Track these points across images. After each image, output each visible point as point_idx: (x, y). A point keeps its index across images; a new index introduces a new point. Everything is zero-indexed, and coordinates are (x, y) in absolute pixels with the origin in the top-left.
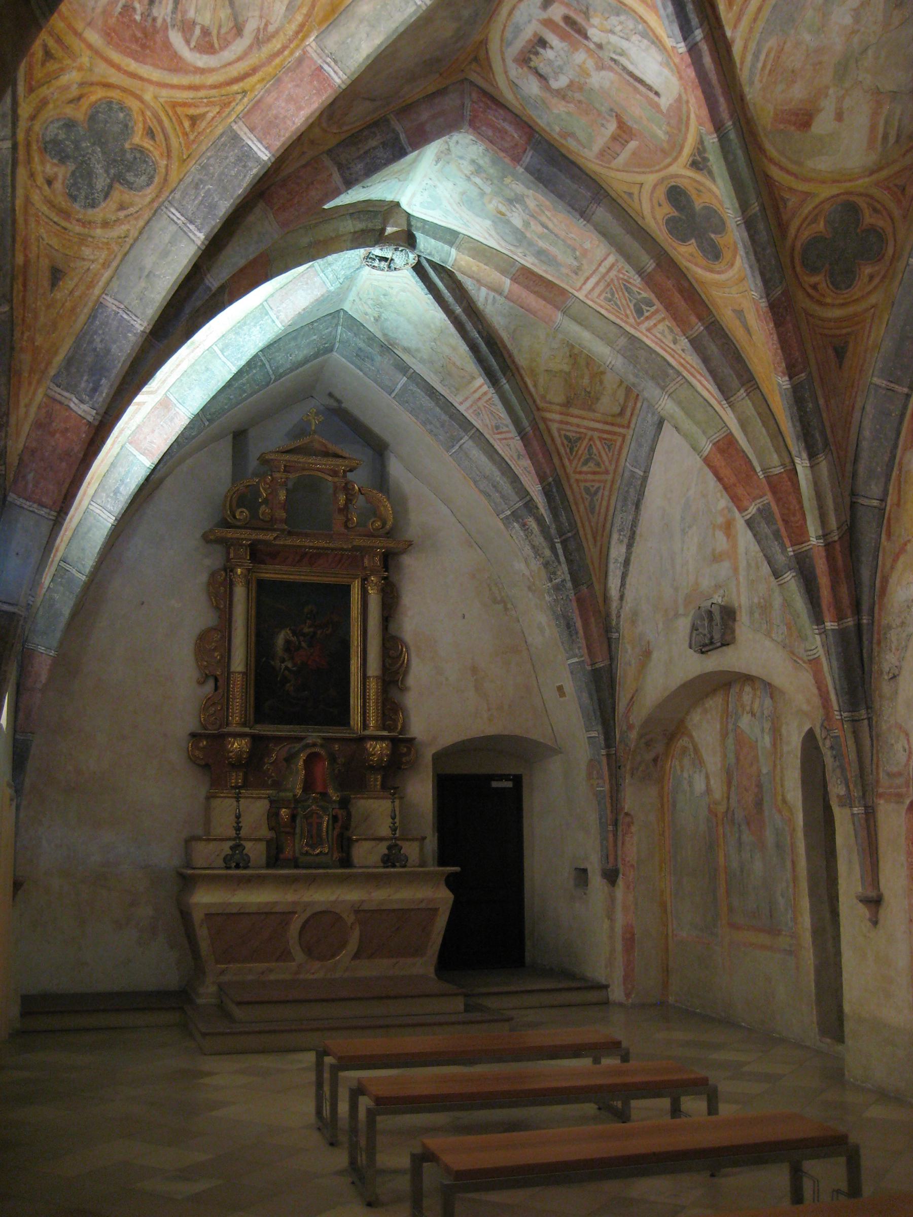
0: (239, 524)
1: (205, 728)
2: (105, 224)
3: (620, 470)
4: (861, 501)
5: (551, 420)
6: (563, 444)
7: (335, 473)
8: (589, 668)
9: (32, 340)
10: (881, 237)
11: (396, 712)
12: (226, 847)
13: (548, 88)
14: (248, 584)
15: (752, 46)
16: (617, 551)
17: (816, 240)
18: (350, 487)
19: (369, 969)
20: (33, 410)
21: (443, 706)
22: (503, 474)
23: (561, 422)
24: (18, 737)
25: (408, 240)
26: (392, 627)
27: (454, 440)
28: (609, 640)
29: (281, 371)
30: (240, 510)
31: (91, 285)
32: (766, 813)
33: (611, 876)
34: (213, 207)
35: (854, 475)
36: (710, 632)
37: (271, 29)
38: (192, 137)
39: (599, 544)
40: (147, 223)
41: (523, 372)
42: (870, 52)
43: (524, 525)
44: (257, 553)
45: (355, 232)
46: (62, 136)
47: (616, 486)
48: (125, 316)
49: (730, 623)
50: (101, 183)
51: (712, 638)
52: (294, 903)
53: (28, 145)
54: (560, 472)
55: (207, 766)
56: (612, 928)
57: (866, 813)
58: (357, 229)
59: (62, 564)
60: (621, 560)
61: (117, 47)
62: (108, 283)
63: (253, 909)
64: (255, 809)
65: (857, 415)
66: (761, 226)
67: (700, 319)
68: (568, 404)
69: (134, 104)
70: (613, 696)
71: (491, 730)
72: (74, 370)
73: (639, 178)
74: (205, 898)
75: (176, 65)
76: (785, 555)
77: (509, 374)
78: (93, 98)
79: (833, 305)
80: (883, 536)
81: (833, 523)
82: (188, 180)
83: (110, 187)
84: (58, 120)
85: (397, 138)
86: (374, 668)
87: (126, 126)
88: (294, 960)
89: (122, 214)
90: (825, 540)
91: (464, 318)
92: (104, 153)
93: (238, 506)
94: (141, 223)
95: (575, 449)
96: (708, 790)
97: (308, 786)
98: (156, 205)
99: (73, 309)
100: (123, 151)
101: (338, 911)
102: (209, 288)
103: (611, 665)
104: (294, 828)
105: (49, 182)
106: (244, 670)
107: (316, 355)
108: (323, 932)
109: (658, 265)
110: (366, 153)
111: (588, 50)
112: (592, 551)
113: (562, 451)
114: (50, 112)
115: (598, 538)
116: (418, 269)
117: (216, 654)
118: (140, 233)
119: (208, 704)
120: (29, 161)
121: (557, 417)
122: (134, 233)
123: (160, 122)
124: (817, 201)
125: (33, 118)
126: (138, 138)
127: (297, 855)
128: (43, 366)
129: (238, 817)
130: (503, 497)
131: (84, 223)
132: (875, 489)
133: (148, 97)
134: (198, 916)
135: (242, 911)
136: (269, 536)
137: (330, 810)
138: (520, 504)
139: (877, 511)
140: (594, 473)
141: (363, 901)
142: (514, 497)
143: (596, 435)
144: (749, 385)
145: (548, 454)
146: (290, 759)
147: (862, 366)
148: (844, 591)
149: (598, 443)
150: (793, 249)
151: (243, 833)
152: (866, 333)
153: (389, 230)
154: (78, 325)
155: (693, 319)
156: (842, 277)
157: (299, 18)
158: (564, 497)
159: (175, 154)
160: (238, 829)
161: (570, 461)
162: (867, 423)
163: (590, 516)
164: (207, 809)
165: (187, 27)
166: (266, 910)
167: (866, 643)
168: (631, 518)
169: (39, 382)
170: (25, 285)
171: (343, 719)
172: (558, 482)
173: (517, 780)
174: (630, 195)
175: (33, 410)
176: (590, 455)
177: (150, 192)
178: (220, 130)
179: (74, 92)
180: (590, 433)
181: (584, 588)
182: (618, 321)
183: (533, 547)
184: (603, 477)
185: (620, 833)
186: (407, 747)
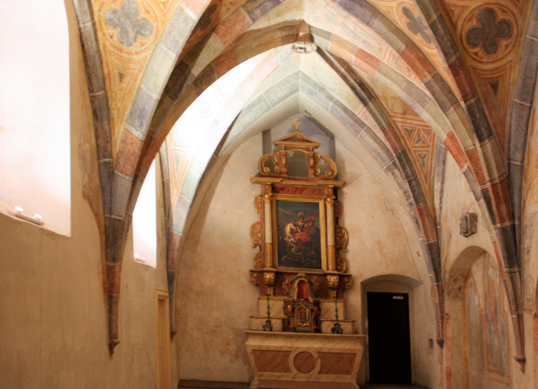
0: (265, 174)
1: (256, 268)
2: (137, 53)
3: (435, 145)
4: (513, 162)
5: (397, 122)
6: (405, 134)
7: (308, 150)
8: (426, 243)
9: (116, 105)
10: (508, 24)
11: (342, 262)
12: (264, 321)
14: (271, 203)
16: (437, 186)
17: (473, 30)
18: (316, 156)
20: (120, 135)
22: (382, 148)
23: (403, 122)
24: (169, 270)
25: (311, 39)
26: (340, 224)
27: (358, 132)
28: (437, 229)
29: (274, 102)
31: (136, 80)
32: (498, 316)
33: (441, 343)
34: (177, 42)
35: (509, 149)
36: (467, 227)
38: (165, 11)
39: (428, 182)
40: (154, 51)
41: (380, 99)
43: (393, 173)
44: (274, 189)
45: (282, 37)
46: (112, 17)
47: (435, 153)
48: (149, 93)
49: (475, 222)
50: (132, 35)
51: (467, 230)
52: (291, 347)
53: (100, 22)
56: (442, 368)
57: (518, 318)
58: (283, 35)
59: (181, 195)
60: (439, 190)
62: (142, 78)
63: (273, 349)
64: (277, 306)
65: (508, 118)
66: (439, 26)
67: (429, 72)
68: (405, 113)
70: (439, 257)
71: (388, 272)
72: (133, 117)
73: (390, 4)
74: (253, 343)
76: (478, 189)
77: (373, 100)
79: (488, 63)
80: (524, 180)
81: (496, 174)
82: (167, 30)
83: (136, 37)
84: (109, 10)
86: (331, 242)
87: (137, 10)
88: (291, 372)
89: (143, 48)
90: (491, 183)
91: (346, 74)
92: (130, 22)
93: (265, 166)
94: (151, 51)
95: (411, 135)
96: (479, 305)
97: (300, 295)
98: (155, 43)
99: (130, 91)
100: (138, 21)
101: (309, 351)
102: (193, 75)
103: (438, 242)
104: (294, 314)
105: (111, 37)
107: (291, 93)
108: (304, 360)
109: (407, 47)
110: (261, 4)
112: (425, 186)
113: (404, 136)
114: (105, 8)
115: (428, 179)
116: (319, 50)
117: (259, 235)
118: (152, 56)
119: (257, 257)
120: (102, 29)
122: (149, 56)
123: (151, 6)
124: (470, 10)
125: (99, 10)
126: (142, 15)
127: (296, 326)
128: (121, 116)
130: (382, 160)
131: (129, 53)
132: (518, 156)
134: (249, 350)
135: (268, 349)
138: (391, 163)
139: (519, 167)
140: (422, 147)
141: (322, 348)
142: (388, 160)
143: (421, 128)
144: (456, 105)
146: (292, 282)
147: (508, 93)
148: (504, 208)
149: (422, 132)
150: (461, 36)
151: (271, 315)
152: (508, 76)
153: (301, 34)
154: (133, 98)
155: (426, 73)
156: (491, 48)
158: (408, 160)
159: (159, 20)
160: (269, 314)
161: (410, 142)
162: (513, 122)
163: (423, 168)
164: (258, 305)
166: (278, 350)
167: (517, 234)
168: (441, 169)
169: (121, 122)
170: (110, 81)
172: (404, 152)
173: (406, 296)
174: (389, 12)
175: (120, 135)
176: (419, 138)
177: (152, 37)
180: (418, 127)
181: (421, 204)
182: (402, 74)
183: (398, 184)
184: (427, 149)
185: (444, 323)
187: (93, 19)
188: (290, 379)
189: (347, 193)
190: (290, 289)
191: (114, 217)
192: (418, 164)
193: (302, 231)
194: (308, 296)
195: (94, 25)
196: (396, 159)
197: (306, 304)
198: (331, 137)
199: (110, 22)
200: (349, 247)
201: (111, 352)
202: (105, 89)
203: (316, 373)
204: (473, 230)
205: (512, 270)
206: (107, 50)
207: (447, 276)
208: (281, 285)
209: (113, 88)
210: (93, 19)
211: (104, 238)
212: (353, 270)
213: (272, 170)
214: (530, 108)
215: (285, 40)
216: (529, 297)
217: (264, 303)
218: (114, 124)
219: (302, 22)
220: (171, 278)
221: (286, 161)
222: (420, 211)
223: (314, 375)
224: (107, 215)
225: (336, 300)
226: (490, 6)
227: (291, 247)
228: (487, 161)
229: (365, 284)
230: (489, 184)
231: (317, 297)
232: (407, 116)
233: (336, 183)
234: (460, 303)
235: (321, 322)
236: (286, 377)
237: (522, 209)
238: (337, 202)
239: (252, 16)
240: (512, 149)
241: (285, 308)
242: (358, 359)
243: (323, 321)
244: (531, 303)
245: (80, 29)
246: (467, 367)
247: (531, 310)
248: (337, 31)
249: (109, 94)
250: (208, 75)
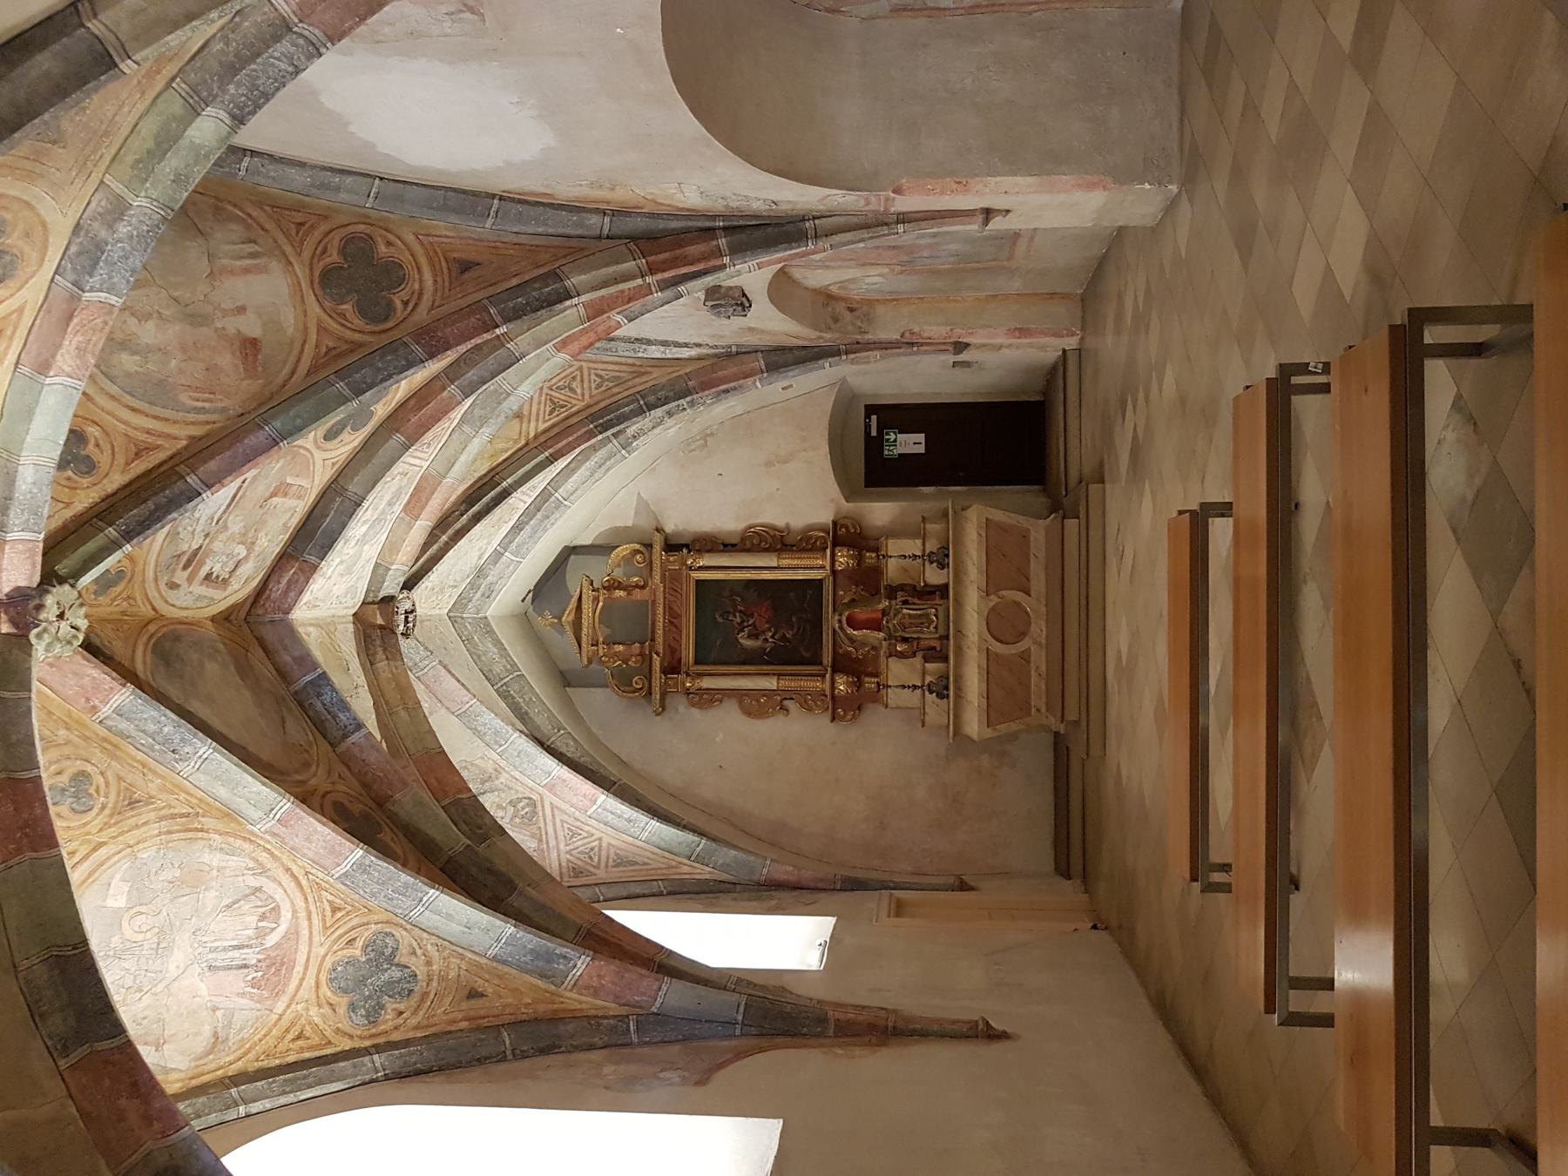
2: (429, 963)
4: (606, 231)
7: (596, 599)
9: (527, 1005)
10: (349, 240)
13: (246, 558)
14: (700, 675)
15: (191, 417)
16: (655, 352)
17: (362, 312)
19: (1038, 581)
21: (806, 494)
31: (480, 966)
33: (960, 347)
34: (406, 885)
37: (251, 865)
42: (176, 294)
44: (673, 667)
50: (396, 973)
53: (372, 1036)
54: (584, 414)
55: (859, 708)
56: (1010, 345)
61: (286, 985)
64: (899, 671)
65: (523, 239)
69: (328, 964)
70: (791, 349)
71: (825, 449)
73: (319, 463)
74: (973, 725)
75: (292, 935)
78: (329, 994)
79: (421, 281)
81: (630, 265)
83: (398, 965)
85: (311, 682)
86: (772, 561)
89: (419, 952)
91: (450, 532)
94: (425, 935)
97: (875, 626)
111: (211, 542)
112: (659, 377)
114: (345, 1026)
116: (409, 584)
119: (806, 706)
121: (533, 424)
122: (434, 940)
125: (351, 1037)
131: (430, 980)
132: (594, 220)
133: (322, 951)
134: (989, 733)
136: (657, 660)
145: (569, 429)
146: (852, 640)
148: (693, 250)
153: (380, 621)
156: (393, 274)
157: (239, 842)
158: (606, 410)
165: (261, 934)
167: (742, 223)
171: (817, 584)
172: (592, 418)
173: (870, 410)
178: (339, 886)
179: (326, 1010)
187: (366, 1052)
188: (1044, 653)
190: (864, 644)
191: (740, 1018)
192: (615, 390)
195: (378, 1049)
196: (609, 433)
198: (569, 552)
199: (373, 1016)
201: (1004, 1036)
202: (497, 1028)
204: (737, 294)
205: (811, 233)
206: (425, 1022)
207: (828, 336)
209: (496, 1012)
210: (366, 1052)
211: (779, 1040)
212: (825, 516)
213: (637, 672)
214: (501, 198)
215: (394, 653)
216: (862, 202)
217: (894, 697)
218: (564, 1010)
219: (357, 617)
220: (854, 885)
222: (705, 386)
223: (1035, 605)
224: (738, 1032)
226: (317, 280)
228: (605, 284)
230: (649, 279)
231: (878, 592)
232: (525, 412)
233: (657, 548)
234: (880, 310)
237: (692, 214)
239: (351, 728)
240: (580, 232)
241: (901, 655)
242: (998, 515)
244: (873, 199)
245: (387, 1078)
246: (1007, 296)
247: (887, 200)
248: (371, 552)
249: (507, 1019)
250: (465, 811)
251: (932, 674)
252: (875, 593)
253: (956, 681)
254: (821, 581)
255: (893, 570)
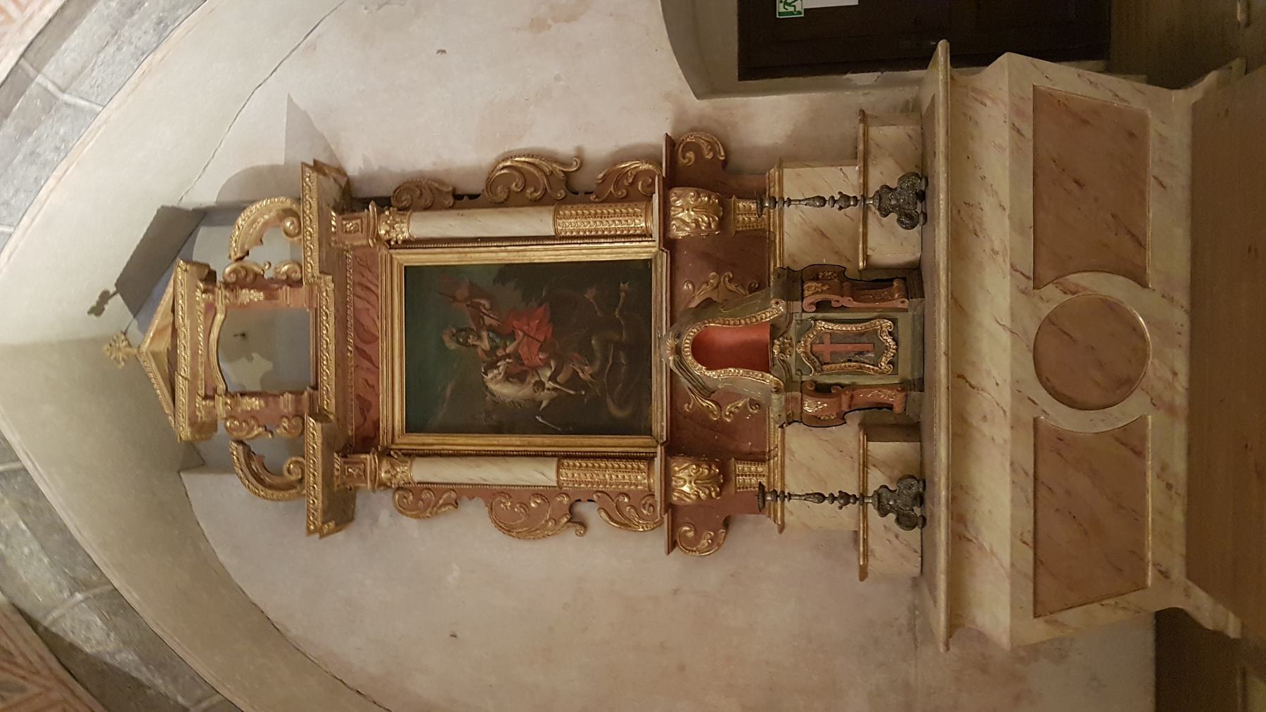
1: (661, 523)
11: (623, 174)
14: (411, 455)
26: (477, 186)
30: (286, 473)
44: (358, 439)
55: (727, 524)
64: (814, 457)
86: (538, 222)
88: (1143, 419)
97: (756, 358)
106: (553, 463)
108: (1080, 358)
129: (821, 497)
134: (1038, 631)
135: (1029, 538)
137: (805, 316)
146: (706, 391)
151: (852, 489)
171: (642, 269)
186: (684, 152)
188: (1180, 430)
189: (365, 160)
193: (512, 336)
194: (761, 325)
197: (792, 333)
200: (564, 147)
203: (1144, 293)
208: (719, 427)
221: (252, 394)
223: (1157, 310)
225: (774, 201)
227: (574, 381)
229: (705, 81)
235: (869, 267)
236: (1167, 446)
238: (398, 200)
241: (816, 422)
243: (866, 257)
251: (882, 465)
252: (760, 285)
253: (953, 500)
254: (647, 262)
255: (795, 233)
